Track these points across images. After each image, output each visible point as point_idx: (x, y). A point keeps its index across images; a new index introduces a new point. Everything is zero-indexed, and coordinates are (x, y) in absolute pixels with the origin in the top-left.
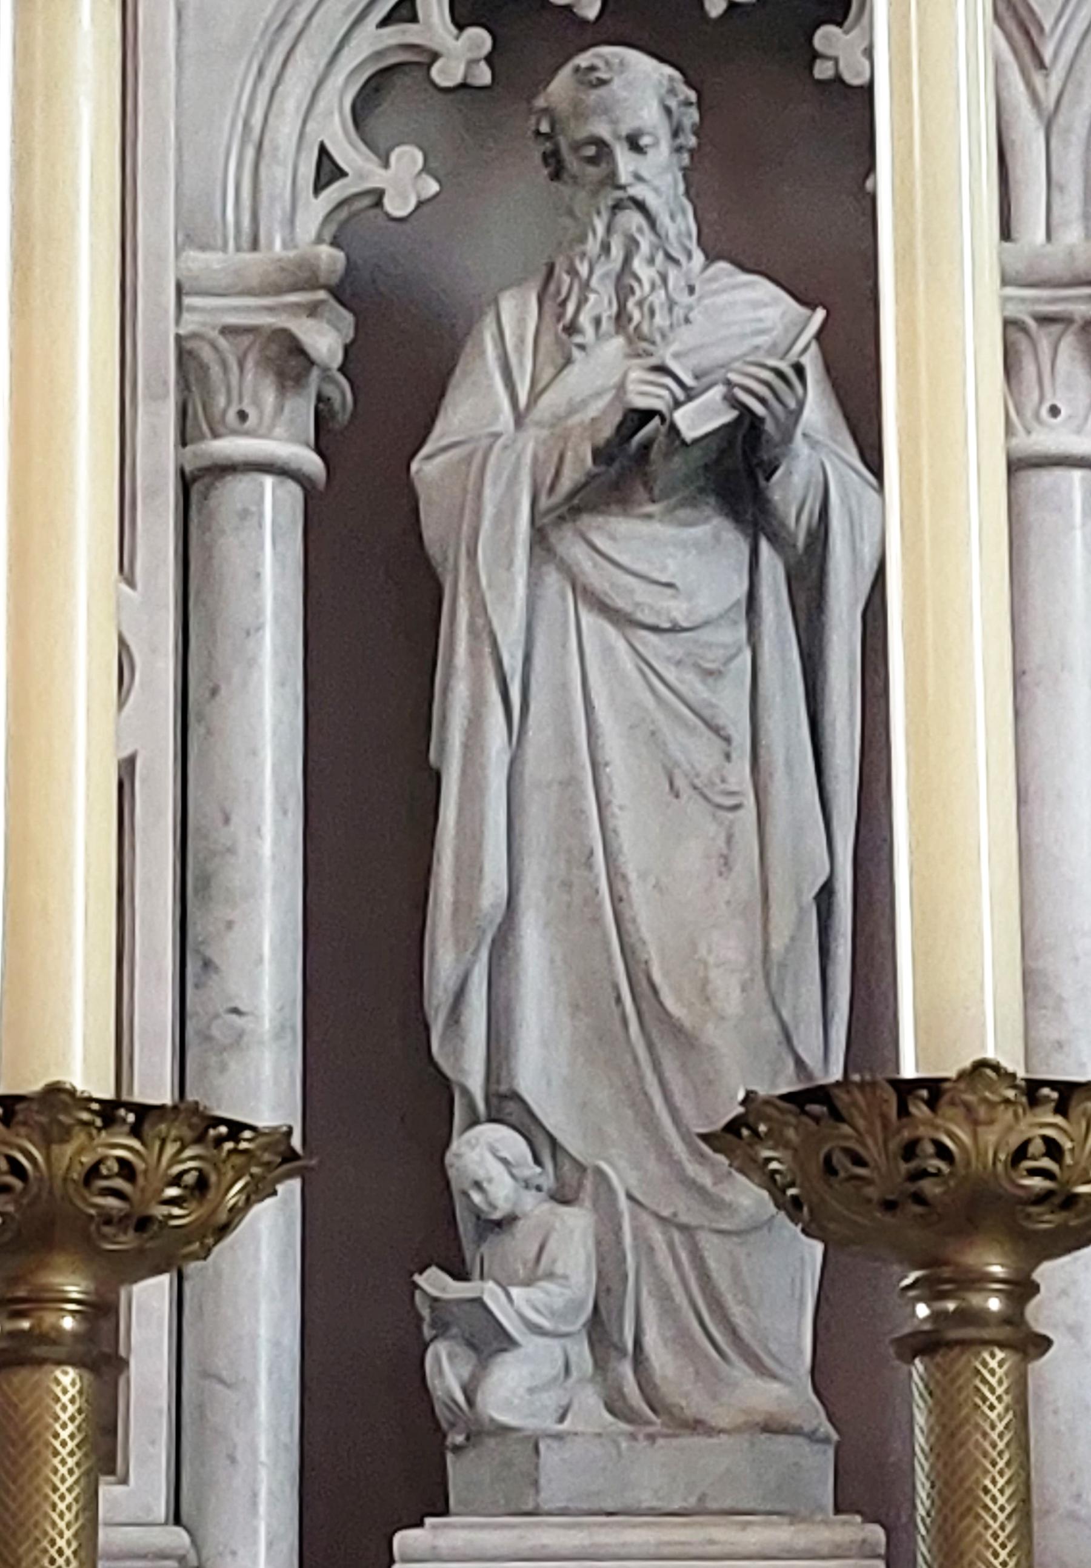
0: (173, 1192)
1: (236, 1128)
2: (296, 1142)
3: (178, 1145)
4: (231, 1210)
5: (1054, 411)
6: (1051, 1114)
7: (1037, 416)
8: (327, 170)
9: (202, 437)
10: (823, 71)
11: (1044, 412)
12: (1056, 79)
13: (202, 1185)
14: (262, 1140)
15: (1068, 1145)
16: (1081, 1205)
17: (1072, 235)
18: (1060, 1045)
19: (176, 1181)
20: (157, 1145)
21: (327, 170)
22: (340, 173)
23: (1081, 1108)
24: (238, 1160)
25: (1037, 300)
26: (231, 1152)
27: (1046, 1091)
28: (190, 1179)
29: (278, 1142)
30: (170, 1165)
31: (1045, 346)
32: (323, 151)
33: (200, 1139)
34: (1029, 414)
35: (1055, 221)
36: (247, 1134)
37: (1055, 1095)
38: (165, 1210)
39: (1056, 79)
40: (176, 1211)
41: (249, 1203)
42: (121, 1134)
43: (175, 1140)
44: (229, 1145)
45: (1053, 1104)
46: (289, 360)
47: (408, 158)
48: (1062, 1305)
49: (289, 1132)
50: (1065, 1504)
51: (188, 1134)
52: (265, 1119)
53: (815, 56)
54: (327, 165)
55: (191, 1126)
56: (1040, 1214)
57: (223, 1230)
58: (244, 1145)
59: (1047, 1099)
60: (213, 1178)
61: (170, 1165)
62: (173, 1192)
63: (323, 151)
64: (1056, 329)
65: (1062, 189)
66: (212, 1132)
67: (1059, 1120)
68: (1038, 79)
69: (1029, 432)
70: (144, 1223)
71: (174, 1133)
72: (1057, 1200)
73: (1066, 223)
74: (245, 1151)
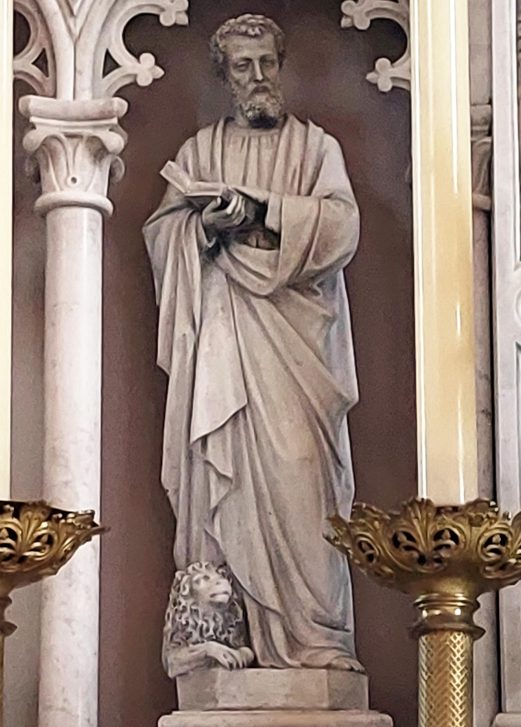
0: (37, 544)
1: (65, 514)
2: (97, 519)
3: (37, 521)
4: (66, 551)
5: (74, 180)
6: (11, 518)
7: (66, 182)
8: (110, 64)
9: (54, 190)
10: (345, 22)
11: (69, 180)
12: (80, 22)
13: (50, 541)
14: (79, 518)
15: (19, 533)
16: (28, 562)
17: (86, 96)
18: (66, 483)
19: (38, 539)
20: (27, 523)
21: (110, 64)
22: (117, 66)
23: (26, 515)
24: (70, 529)
25: (65, 127)
26: (63, 524)
27: (8, 506)
28: (45, 538)
29: (88, 519)
30: (35, 531)
31: (70, 150)
32: (108, 55)
33: (49, 519)
34: (62, 180)
35: (78, 89)
36: (71, 515)
37: (12, 509)
38: (32, 553)
39: (80, 22)
40: (38, 554)
41: (74, 547)
42: (8, 517)
43: (36, 519)
44: (63, 521)
45: (11, 513)
46: (99, 151)
47: (148, 59)
48: (62, 608)
49: (92, 514)
50: (60, 703)
51: (42, 517)
52: (82, 507)
53: (342, 15)
54: (109, 61)
55: (43, 513)
56: (8, 565)
57: (63, 560)
58: (70, 521)
59: (9, 510)
60: (56, 538)
61: (35, 531)
62: (37, 544)
63: (108, 55)
64: (75, 140)
65: (81, 74)
66: (55, 516)
67: (15, 520)
68: (71, 21)
69: (61, 190)
70: (23, 559)
71: (35, 516)
72: (16, 559)
73: (83, 90)
74: (72, 524)
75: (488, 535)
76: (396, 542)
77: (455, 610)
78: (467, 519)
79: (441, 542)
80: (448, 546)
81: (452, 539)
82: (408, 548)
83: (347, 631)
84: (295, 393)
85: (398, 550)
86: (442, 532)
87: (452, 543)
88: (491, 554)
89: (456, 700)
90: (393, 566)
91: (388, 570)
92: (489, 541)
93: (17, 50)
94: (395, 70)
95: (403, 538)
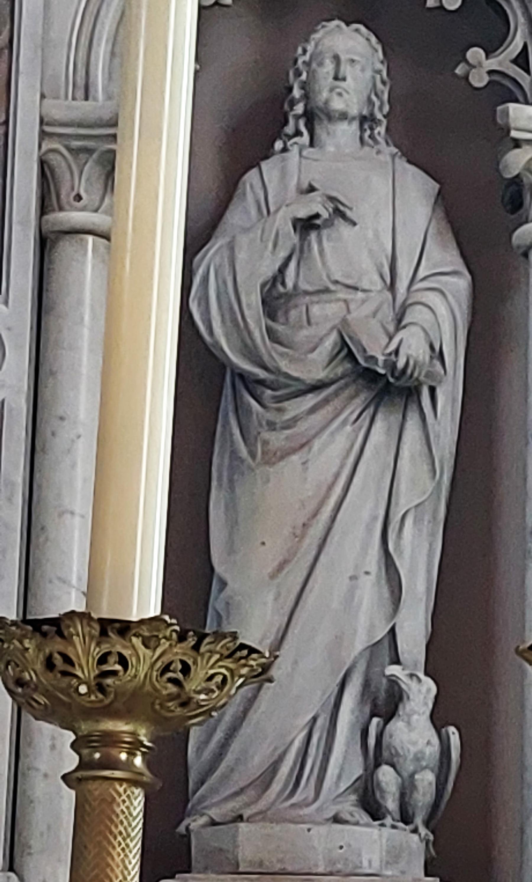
22: (515, 61)
75: (166, 659)
76: (49, 664)
77: (120, 752)
78: (140, 639)
79: (106, 668)
80: (114, 673)
81: (120, 663)
82: (65, 674)
83: (397, 153)
84: (358, 103)
85: (51, 675)
86: (109, 653)
87: (118, 667)
88: (169, 685)
89: (117, 840)
90: (46, 694)
91: (42, 700)
92: (166, 669)
93: (526, 68)
94: (490, 61)
95: (58, 660)
